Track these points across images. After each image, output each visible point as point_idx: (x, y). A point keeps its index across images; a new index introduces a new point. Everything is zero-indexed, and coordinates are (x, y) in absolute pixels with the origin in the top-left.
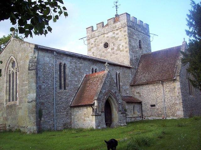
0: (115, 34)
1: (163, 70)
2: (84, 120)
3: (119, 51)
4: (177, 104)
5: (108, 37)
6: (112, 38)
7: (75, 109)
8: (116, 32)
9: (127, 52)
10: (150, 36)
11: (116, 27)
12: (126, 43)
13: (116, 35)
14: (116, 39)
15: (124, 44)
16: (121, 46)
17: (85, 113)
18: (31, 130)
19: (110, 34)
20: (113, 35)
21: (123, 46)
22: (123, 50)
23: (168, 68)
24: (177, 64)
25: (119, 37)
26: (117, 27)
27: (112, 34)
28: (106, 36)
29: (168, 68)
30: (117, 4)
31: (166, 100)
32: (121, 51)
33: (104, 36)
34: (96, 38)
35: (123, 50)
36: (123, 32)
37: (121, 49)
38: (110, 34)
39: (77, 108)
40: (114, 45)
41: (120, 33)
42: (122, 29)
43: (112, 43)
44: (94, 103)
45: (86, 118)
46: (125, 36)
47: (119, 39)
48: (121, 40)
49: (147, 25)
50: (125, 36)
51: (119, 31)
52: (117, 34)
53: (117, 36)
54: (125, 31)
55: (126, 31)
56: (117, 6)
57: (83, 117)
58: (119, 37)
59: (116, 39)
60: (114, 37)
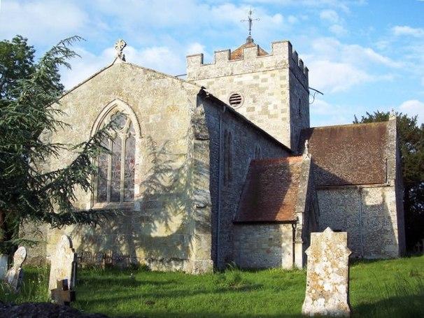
0: (260, 80)
1: (358, 164)
2: (268, 252)
3: (267, 116)
4: (388, 231)
5: (240, 83)
6: (251, 86)
7: (244, 227)
8: (262, 76)
9: (284, 119)
10: (309, 93)
11: (262, 65)
12: (283, 102)
13: (260, 83)
14: (262, 91)
15: (278, 103)
16: (270, 107)
17: (272, 237)
18: (202, 267)
19: (248, 79)
20: (255, 82)
21: (276, 107)
22: (275, 116)
23: (368, 162)
24: (386, 156)
25: (267, 88)
26: (265, 66)
27: (252, 78)
28: (236, 79)
29: (368, 162)
30: (252, 17)
31: (365, 223)
32: (271, 117)
33: (231, 81)
34: (211, 80)
35: (275, 116)
36: (278, 79)
37: (272, 113)
38: (248, 79)
39: (251, 227)
40: (254, 102)
41: (270, 80)
42: (276, 72)
43: (252, 96)
44: (298, 218)
45: (272, 248)
46: (282, 86)
47: (267, 91)
48: (272, 94)
49: (307, 70)
50: (282, 86)
51: (268, 75)
52: (264, 80)
53: (262, 85)
54: (283, 78)
55: (285, 77)
56: (250, 21)
57: (265, 246)
58: (267, 88)
59: (262, 91)
60: (257, 85)
